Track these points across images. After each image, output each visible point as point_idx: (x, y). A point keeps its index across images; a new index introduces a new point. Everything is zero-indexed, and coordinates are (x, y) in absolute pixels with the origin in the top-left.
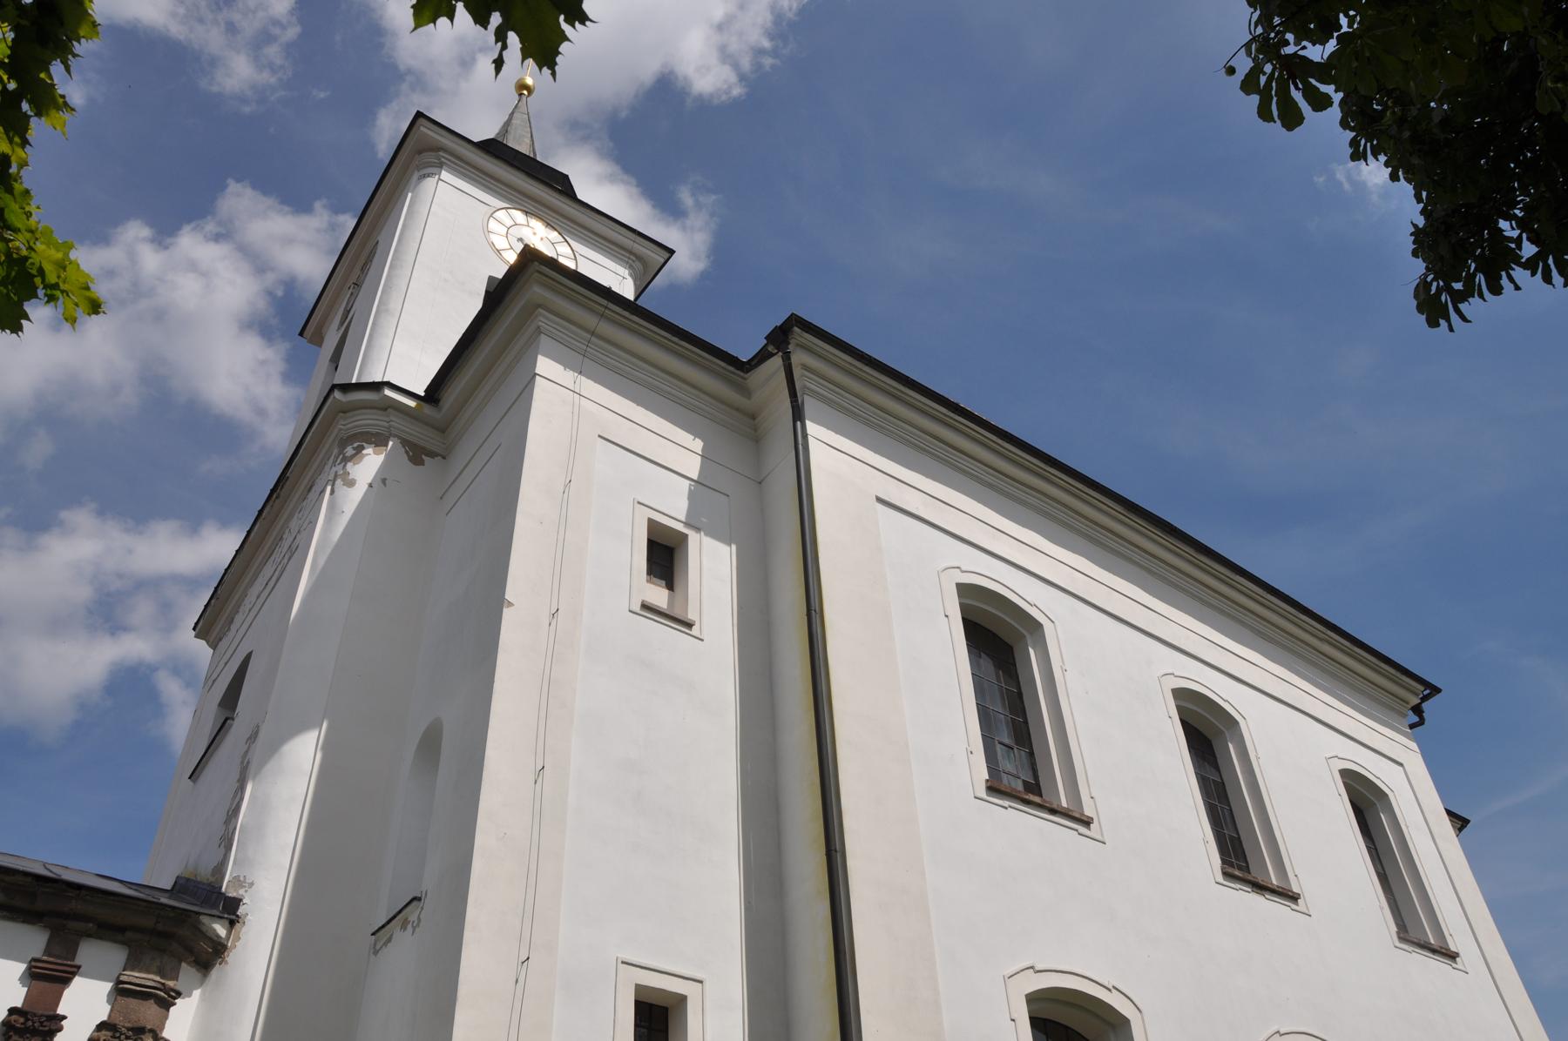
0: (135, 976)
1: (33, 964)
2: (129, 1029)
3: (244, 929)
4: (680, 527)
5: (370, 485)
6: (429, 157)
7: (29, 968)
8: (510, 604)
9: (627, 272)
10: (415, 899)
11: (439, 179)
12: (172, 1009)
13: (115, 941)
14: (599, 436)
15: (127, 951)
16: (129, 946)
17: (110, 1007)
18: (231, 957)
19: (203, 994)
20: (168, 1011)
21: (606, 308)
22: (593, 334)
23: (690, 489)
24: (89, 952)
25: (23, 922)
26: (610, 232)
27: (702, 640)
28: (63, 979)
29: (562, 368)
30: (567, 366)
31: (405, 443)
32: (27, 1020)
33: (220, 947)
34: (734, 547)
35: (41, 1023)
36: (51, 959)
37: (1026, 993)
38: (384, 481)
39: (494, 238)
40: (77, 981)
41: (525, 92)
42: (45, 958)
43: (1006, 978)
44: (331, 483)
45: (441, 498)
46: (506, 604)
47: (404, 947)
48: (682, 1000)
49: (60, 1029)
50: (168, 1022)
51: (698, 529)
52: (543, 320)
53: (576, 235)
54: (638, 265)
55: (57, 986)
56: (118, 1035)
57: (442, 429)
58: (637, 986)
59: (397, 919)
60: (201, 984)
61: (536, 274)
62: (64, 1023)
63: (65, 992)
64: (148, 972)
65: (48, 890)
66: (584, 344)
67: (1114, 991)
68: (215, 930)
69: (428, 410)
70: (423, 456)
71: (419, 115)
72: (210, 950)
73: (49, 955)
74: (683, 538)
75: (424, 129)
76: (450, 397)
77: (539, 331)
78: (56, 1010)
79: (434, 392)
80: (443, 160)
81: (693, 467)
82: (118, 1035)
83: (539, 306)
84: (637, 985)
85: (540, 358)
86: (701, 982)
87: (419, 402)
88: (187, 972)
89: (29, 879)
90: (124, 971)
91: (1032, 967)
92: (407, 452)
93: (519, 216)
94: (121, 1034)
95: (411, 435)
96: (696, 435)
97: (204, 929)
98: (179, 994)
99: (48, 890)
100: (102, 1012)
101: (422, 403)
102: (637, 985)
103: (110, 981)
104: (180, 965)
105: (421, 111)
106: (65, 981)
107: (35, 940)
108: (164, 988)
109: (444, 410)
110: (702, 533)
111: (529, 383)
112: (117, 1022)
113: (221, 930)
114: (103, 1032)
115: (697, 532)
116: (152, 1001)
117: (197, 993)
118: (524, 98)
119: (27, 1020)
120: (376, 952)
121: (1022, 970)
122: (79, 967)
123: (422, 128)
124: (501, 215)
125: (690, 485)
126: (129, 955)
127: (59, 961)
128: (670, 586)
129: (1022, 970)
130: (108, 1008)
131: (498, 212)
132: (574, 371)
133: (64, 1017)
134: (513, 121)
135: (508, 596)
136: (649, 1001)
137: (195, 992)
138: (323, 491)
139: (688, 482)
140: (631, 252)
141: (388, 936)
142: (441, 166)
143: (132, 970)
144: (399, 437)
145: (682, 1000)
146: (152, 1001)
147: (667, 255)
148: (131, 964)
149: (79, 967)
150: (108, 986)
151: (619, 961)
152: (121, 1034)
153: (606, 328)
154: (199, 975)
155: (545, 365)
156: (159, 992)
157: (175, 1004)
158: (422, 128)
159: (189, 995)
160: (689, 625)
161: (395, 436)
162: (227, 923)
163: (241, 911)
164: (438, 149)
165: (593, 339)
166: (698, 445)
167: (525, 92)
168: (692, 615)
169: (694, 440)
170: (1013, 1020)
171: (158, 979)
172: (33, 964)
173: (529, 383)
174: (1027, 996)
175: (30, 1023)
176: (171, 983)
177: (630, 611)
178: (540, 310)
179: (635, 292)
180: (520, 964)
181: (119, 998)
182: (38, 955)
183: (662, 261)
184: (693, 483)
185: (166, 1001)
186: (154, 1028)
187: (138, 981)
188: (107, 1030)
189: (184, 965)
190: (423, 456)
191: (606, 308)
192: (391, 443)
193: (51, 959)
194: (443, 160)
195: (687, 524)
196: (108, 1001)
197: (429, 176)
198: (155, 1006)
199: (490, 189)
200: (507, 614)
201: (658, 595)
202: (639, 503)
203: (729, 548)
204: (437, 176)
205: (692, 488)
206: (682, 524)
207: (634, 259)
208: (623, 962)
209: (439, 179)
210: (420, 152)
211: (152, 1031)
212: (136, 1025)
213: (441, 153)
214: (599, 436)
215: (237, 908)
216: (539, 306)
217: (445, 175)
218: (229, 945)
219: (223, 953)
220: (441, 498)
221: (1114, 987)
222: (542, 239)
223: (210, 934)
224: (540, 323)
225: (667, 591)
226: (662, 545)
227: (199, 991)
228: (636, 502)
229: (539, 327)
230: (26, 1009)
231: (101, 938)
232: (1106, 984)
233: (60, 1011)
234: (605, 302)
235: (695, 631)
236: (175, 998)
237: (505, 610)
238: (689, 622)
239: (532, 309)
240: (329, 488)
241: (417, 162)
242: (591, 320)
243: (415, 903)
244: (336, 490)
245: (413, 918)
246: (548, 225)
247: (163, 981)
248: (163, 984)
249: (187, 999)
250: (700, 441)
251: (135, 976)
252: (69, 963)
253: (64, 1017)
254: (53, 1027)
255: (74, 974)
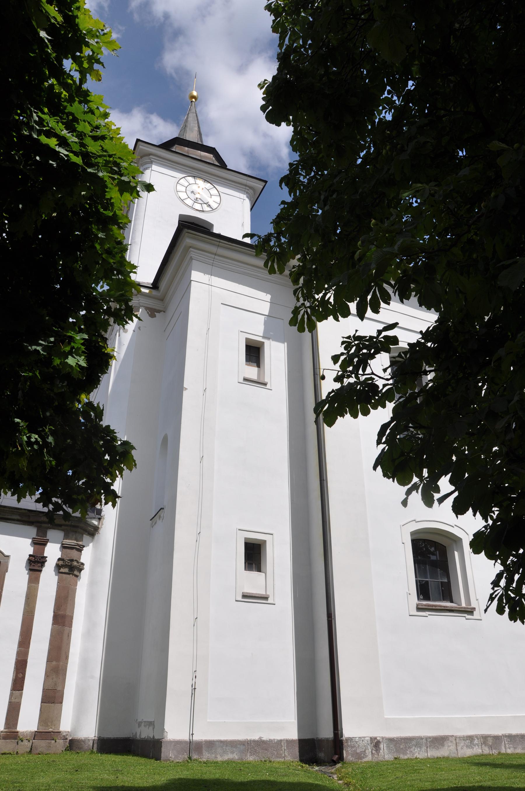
0: (68, 542)
1: (34, 539)
2: (68, 560)
3: (104, 521)
4: (260, 339)
5: (134, 331)
6: (146, 159)
7: (33, 541)
8: (186, 389)
9: (245, 196)
10: (161, 509)
11: (152, 170)
12: (82, 551)
13: (59, 530)
14: (222, 304)
15: (64, 533)
16: (64, 531)
17: (61, 553)
18: (101, 531)
19: (93, 545)
20: (81, 552)
21: (220, 242)
22: (215, 254)
23: (265, 320)
24: (51, 534)
25: (28, 525)
26: (236, 178)
27: (272, 390)
28: (44, 544)
29: (203, 274)
30: (205, 273)
31: (147, 308)
32: (35, 558)
33: (96, 528)
34: (286, 344)
35: (40, 559)
36: (39, 538)
37: (411, 531)
38: (139, 328)
39: (180, 194)
40: (49, 544)
41: (194, 100)
42: (37, 537)
43: (401, 526)
44: (118, 331)
45: (165, 331)
46: (184, 389)
47: (160, 524)
48: (265, 542)
49: (46, 561)
50: (82, 556)
51: (268, 339)
52: (193, 253)
53: (219, 183)
54: (251, 191)
55: (42, 546)
56: (65, 562)
57: (162, 300)
58: (245, 538)
59: (157, 515)
60: (92, 541)
61: (186, 234)
62: (47, 559)
63: (45, 548)
64: (72, 540)
65: (33, 514)
66: (212, 260)
67: (455, 527)
68: (93, 523)
69: (154, 292)
70: (155, 313)
71: (138, 140)
72: (93, 530)
73: (38, 536)
74: (263, 343)
75: (141, 146)
76: (163, 285)
77: (191, 259)
78: (44, 555)
79: (155, 285)
80: (152, 159)
81: (266, 308)
82: (65, 562)
83: (190, 247)
84: (245, 538)
85: (192, 271)
86: (272, 534)
87: (150, 289)
88: (86, 537)
89: (26, 511)
90: (64, 540)
91: (415, 520)
92: (148, 313)
93: (191, 180)
94: (66, 562)
95: (149, 304)
96: (267, 292)
97: (89, 523)
98: (84, 546)
99: (33, 514)
100: (59, 555)
101: (152, 290)
102: (245, 538)
103: (60, 544)
104: (83, 536)
105: (138, 138)
106: (45, 545)
107: (33, 531)
108: (78, 545)
109: (161, 291)
110: (271, 340)
111: (189, 284)
112: (64, 558)
113: (95, 522)
114: (60, 561)
115: (268, 340)
116: (75, 550)
117: (91, 545)
118: (193, 103)
119: (35, 558)
120: (152, 527)
121: (409, 522)
122: (48, 540)
123: (140, 147)
124: (182, 181)
125: (265, 318)
126: (65, 534)
127: (42, 538)
128: (258, 366)
129: (409, 522)
130: (61, 553)
131: (180, 181)
132: (208, 275)
133: (47, 557)
134: (189, 119)
135: (185, 386)
136: (253, 543)
137: (90, 544)
138: (116, 334)
139: (264, 317)
140: (246, 186)
141: (155, 522)
142: (151, 162)
143: (66, 539)
144: (144, 307)
145: (265, 542)
146: (75, 550)
147: (264, 184)
148: (66, 537)
149: (48, 540)
150: (59, 546)
151: (238, 529)
152: (66, 562)
153: (221, 251)
154: (91, 538)
155: (195, 275)
156: (76, 547)
157: (83, 550)
158: (140, 147)
159: (88, 546)
160: (265, 384)
161: (142, 306)
162: (97, 520)
163: (103, 514)
164: (150, 154)
165: (216, 257)
166: (268, 297)
167: (194, 100)
168: (267, 380)
169: (266, 295)
170: (403, 543)
171: (75, 542)
172: (34, 539)
173: (189, 284)
174: (411, 533)
175: (36, 559)
176: (80, 543)
177: (239, 382)
178: (191, 249)
179: (251, 204)
180: (198, 534)
181: (63, 549)
182: (35, 536)
183: (262, 187)
184: (266, 317)
185: (80, 550)
186: (76, 559)
187: (69, 543)
188: (61, 561)
189: (84, 535)
190: (155, 313)
191: (220, 242)
192: (140, 310)
193: (39, 538)
194: (152, 159)
195: (263, 337)
196: (60, 551)
197: (147, 169)
198: (76, 551)
199: (176, 169)
200: (185, 393)
201: (252, 372)
202: (241, 332)
203: (284, 344)
204: (151, 168)
205: (266, 319)
206: (261, 338)
207: (248, 188)
208: (239, 530)
209: (152, 170)
210: (141, 157)
211: (76, 560)
212: (71, 559)
213: (151, 156)
214: (222, 304)
215: (101, 513)
216: (190, 247)
217: (154, 167)
218: (100, 527)
219: (98, 530)
220: (165, 331)
221: (455, 525)
222: (203, 189)
223: (91, 524)
224: (192, 255)
225: (257, 368)
226: (256, 347)
227: (92, 543)
228: (240, 331)
229: (191, 257)
230: (35, 555)
231: (54, 529)
232: (452, 524)
233: (45, 555)
234: (219, 240)
235: (268, 386)
236: (83, 548)
237: (184, 392)
238: (265, 383)
239: (188, 248)
240: (118, 334)
241: (141, 163)
242: (213, 249)
243: (162, 510)
244: (120, 334)
245: (162, 516)
246: (205, 181)
247: (77, 543)
248: (77, 544)
249: (87, 547)
250: (269, 295)
251: (68, 542)
252: (45, 538)
253: (47, 557)
254: (44, 561)
255: (47, 542)
